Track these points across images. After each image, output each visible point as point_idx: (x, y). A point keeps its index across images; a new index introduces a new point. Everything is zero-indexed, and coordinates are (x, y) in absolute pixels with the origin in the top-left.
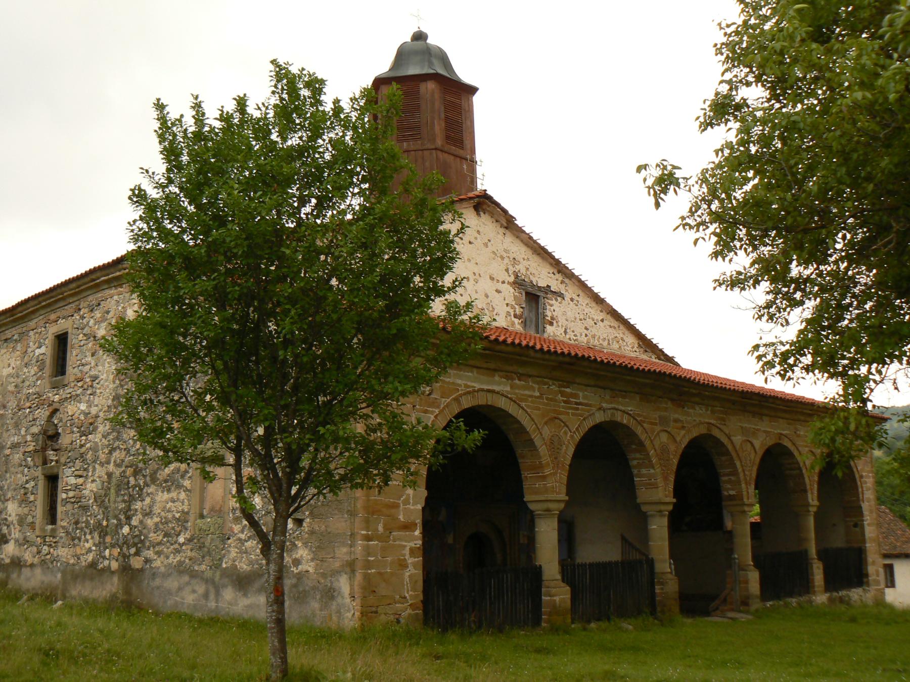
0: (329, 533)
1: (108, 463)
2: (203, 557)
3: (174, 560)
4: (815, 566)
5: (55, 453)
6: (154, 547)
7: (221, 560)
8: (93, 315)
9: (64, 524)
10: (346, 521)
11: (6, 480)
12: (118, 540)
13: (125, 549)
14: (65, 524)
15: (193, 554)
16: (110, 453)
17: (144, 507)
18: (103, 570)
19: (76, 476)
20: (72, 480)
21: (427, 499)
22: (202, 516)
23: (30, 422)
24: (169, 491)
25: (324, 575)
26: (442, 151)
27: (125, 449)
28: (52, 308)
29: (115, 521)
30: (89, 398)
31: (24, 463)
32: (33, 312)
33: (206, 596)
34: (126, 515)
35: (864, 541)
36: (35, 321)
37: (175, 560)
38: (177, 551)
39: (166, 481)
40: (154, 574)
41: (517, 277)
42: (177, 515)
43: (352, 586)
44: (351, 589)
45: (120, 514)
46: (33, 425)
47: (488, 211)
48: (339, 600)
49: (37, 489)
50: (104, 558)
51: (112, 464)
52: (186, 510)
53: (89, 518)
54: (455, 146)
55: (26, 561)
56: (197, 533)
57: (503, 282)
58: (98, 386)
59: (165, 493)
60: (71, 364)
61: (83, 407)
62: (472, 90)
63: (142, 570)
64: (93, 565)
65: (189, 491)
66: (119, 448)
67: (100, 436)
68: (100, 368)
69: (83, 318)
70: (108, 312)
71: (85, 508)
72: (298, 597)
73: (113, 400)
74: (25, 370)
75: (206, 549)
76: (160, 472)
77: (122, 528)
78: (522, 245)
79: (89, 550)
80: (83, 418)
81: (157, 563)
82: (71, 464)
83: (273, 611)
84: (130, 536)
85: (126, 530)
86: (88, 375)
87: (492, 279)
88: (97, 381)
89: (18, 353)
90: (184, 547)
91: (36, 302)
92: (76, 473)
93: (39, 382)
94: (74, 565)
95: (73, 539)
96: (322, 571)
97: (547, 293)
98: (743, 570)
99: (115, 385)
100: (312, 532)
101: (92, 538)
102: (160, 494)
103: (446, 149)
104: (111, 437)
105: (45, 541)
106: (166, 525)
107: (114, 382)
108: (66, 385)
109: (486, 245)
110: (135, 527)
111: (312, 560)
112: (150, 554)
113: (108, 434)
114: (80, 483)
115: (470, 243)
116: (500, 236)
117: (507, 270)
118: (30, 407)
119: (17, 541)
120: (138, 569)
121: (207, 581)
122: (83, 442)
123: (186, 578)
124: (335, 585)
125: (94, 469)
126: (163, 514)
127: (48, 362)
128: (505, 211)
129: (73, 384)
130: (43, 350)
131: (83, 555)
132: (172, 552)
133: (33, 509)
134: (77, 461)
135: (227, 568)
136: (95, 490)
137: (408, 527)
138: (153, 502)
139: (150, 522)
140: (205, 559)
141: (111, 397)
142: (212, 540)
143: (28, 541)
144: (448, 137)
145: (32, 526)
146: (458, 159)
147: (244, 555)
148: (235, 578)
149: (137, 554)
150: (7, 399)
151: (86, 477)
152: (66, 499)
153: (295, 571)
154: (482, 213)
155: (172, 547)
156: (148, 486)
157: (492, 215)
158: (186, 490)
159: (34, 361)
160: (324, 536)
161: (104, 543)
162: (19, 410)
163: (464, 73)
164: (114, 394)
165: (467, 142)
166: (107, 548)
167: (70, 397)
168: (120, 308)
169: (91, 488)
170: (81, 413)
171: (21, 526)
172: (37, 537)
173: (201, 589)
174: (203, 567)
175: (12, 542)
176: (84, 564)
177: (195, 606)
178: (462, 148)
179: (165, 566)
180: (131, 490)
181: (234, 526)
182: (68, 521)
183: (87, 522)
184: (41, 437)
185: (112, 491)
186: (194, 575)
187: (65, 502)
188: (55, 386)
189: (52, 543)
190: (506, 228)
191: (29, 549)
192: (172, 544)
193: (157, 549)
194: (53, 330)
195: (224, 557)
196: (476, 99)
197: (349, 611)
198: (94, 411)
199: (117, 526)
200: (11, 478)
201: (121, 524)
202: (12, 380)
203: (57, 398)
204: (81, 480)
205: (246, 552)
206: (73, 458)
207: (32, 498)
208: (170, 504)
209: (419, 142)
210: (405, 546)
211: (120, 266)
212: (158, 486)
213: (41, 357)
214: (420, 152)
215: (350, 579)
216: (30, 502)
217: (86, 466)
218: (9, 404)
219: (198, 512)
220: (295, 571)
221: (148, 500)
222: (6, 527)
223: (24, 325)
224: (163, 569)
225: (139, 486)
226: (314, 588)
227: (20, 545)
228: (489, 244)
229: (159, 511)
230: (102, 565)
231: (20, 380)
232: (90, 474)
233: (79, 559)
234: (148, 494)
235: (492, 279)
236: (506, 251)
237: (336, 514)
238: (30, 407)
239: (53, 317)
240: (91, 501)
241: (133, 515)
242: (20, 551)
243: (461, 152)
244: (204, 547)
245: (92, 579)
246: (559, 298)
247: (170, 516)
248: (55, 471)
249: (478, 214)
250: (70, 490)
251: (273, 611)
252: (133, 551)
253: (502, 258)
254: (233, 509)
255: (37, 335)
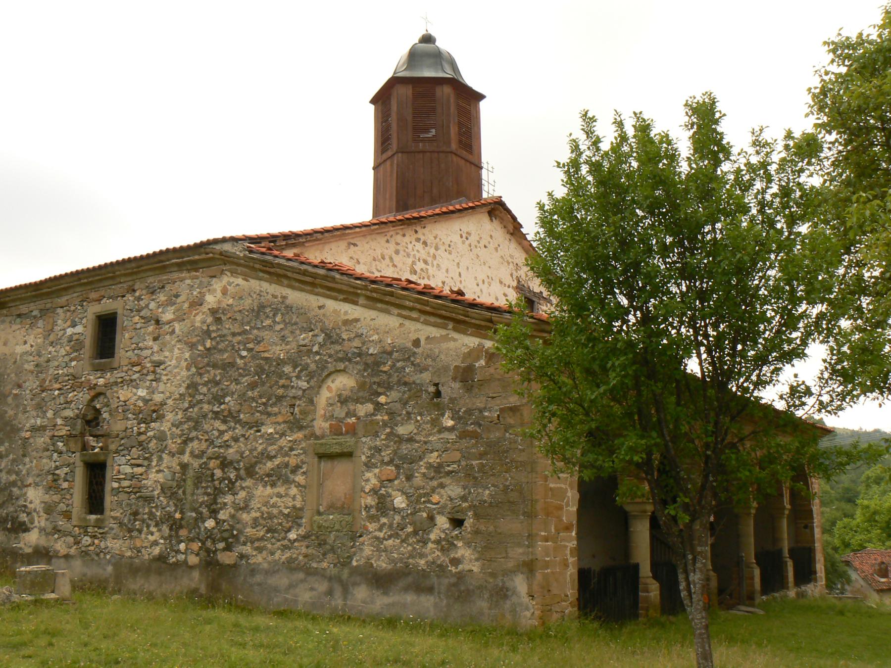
0: (500, 534)
1: (182, 452)
2: (324, 554)
3: (281, 556)
4: (789, 563)
5: (95, 439)
6: (252, 542)
7: (350, 558)
8: (154, 297)
9: (117, 514)
10: (522, 522)
11: (25, 464)
12: (198, 534)
13: (209, 543)
14: (118, 514)
15: (310, 551)
16: (185, 442)
17: (237, 501)
18: (177, 564)
19: (132, 465)
20: (128, 469)
21: (580, 501)
22: (319, 513)
23: (60, 404)
24: (273, 485)
25: (493, 575)
26: (455, 154)
27: (206, 440)
28: (93, 286)
29: (194, 515)
30: (151, 384)
31: (52, 448)
32: (65, 289)
33: (330, 592)
34: (209, 508)
35: (814, 543)
36: (65, 298)
37: (284, 557)
38: (285, 548)
39: (268, 475)
40: (253, 570)
41: (519, 282)
42: (286, 511)
43: (530, 586)
44: (528, 588)
45: (200, 506)
46: (65, 408)
47: (499, 217)
48: (514, 599)
49: (73, 476)
50: (178, 552)
51: (187, 454)
52: (298, 506)
53: (154, 510)
54: (466, 151)
55: (57, 552)
56: (316, 529)
57: (509, 287)
58: (165, 373)
59: (268, 488)
60: (122, 346)
61: (142, 393)
62: (480, 97)
63: (235, 566)
64: (161, 558)
65: (305, 487)
66: (198, 438)
67: (169, 424)
68: (167, 354)
69: (139, 299)
70: (177, 296)
71: (148, 499)
72: (458, 596)
73: (188, 387)
74: (51, 349)
75: (328, 547)
76: (259, 466)
77: (204, 522)
78: (523, 251)
79: (155, 543)
80: (141, 405)
81: (259, 559)
82: (125, 452)
83: (703, 618)
84: (216, 531)
85: (210, 523)
86: (148, 359)
87: (501, 282)
88: (162, 367)
89: (40, 330)
90: (296, 544)
91: (75, 278)
92: (133, 461)
93: (74, 363)
94: (131, 557)
95: (130, 531)
96: (490, 570)
97: (540, 299)
98: (749, 567)
99: (190, 373)
100: (477, 532)
101: (159, 530)
102: (260, 488)
103: (458, 153)
104: (186, 426)
105: (86, 531)
106: (269, 521)
107: (188, 369)
108: (115, 369)
109: (496, 249)
110: (224, 521)
111: (477, 560)
112: (247, 549)
113: (181, 423)
114: (140, 473)
115: (485, 247)
116: (507, 242)
117: (512, 275)
118: (59, 389)
119: (42, 530)
120: (229, 565)
121: (330, 579)
122: (142, 430)
123: (301, 575)
124: (508, 584)
125: (160, 459)
126: (264, 509)
127: (88, 342)
128: (514, 218)
129: (125, 368)
130: (79, 329)
131: (146, 547)
132: (279, 549)
133: (68, 497)
134: (134, 449)
135: (357, 566)
136: (161, 480)
137: (568, 528)
138: (250, 497)
139: (245, 517)
140: (327, 556)
141: (185, 385)
142: (337, 537)
143: (59, 531)
144: (460, 142)
145: (67, 515)
146: (468, 164)
147: (383, 554)
148: (370, 576)
149: (228, 548)
150: (24, 378)
151: (149, 467)
152: (118, 488)
153: (454, 571)
154: (494, 219)
155: (279, 543)
156: (242, 479)
157: (502, 220)
158: (298, 485)
159: (65, 340)
160: (493, 536)
161: (177, 536)
162: (43, 391)
163: (471, 79)
164: (188, 382)
165: (475, 148)
166: (182, 541)
167: (122, 382)
168: (195, 293)
169: (154, 479)
170: (138, 399)
171: (48, 514)
172: (75, 526)
173: (323, 587)
174: (325, 565)
175: (36, 530)
176: (147, 557)
177: (313, 604)
178: (471, 153)
179: (269, 563)
180: (216, 483)
181: (368, 524)
182: (121, 511)
183: (151, 514)
184: (79, 421)
185: (189, 482)
186: (310, 572)
187: (116, 492)
188: (98, 369)
189: (97, 534)
190: (512, 234)
191: (63, 539)
192: (279, 540)
193: (256, 544)
194: (94, 309)
195: (355, 555)
196: (482, 104)
197: (527, 609)
198: (158, 398)
199: (196, 519)
200: (32, 462)
201: (202, 518)
202: (31, 358)
203: (101, 381)
204: (140, 470)
205: (385, 550)
206: (128, 446)
207: (65, 485)
208: (275, 499)
209: (435, 144)
210: (567, 546)
211: (202, 250)
212: (257, 479)
213: (75, 337)
214: (436, 154)
215: (528, 579)
216: (62, 489)
217: (147, 455)
218: (27, 384)
219: (315, 508)
220: (454, 571)
221: (242, 494)
222: (25, 515)
223: (49, 301)
224: (266, 565)
225: (230, 480)
226: (480, 588)
227: (47, 534)
228: (499, 249)
229: (259, 506)
230: (174, 559)
231: (42, 360)
232: (154, 463)
233: (139, 551)
234: (243, 488)
235: (501, 282)
236: (511, 256)
237: (508, 515)
238: (59, 389)
239: (93, 295)
240: (156, 493)
241: (221, 509)
242: (48, 540)
243: (469, 157)
244: (325, 544)
245: (160, 573)
246: (548, 304)
247: (275, 511)
248: (102, 458)
249: (492, 220)
250: (124, 479)
251: (703, 618)
252: (221, 545)
253: (509, 263)
254: (366, 506)
255: (69, 314)
